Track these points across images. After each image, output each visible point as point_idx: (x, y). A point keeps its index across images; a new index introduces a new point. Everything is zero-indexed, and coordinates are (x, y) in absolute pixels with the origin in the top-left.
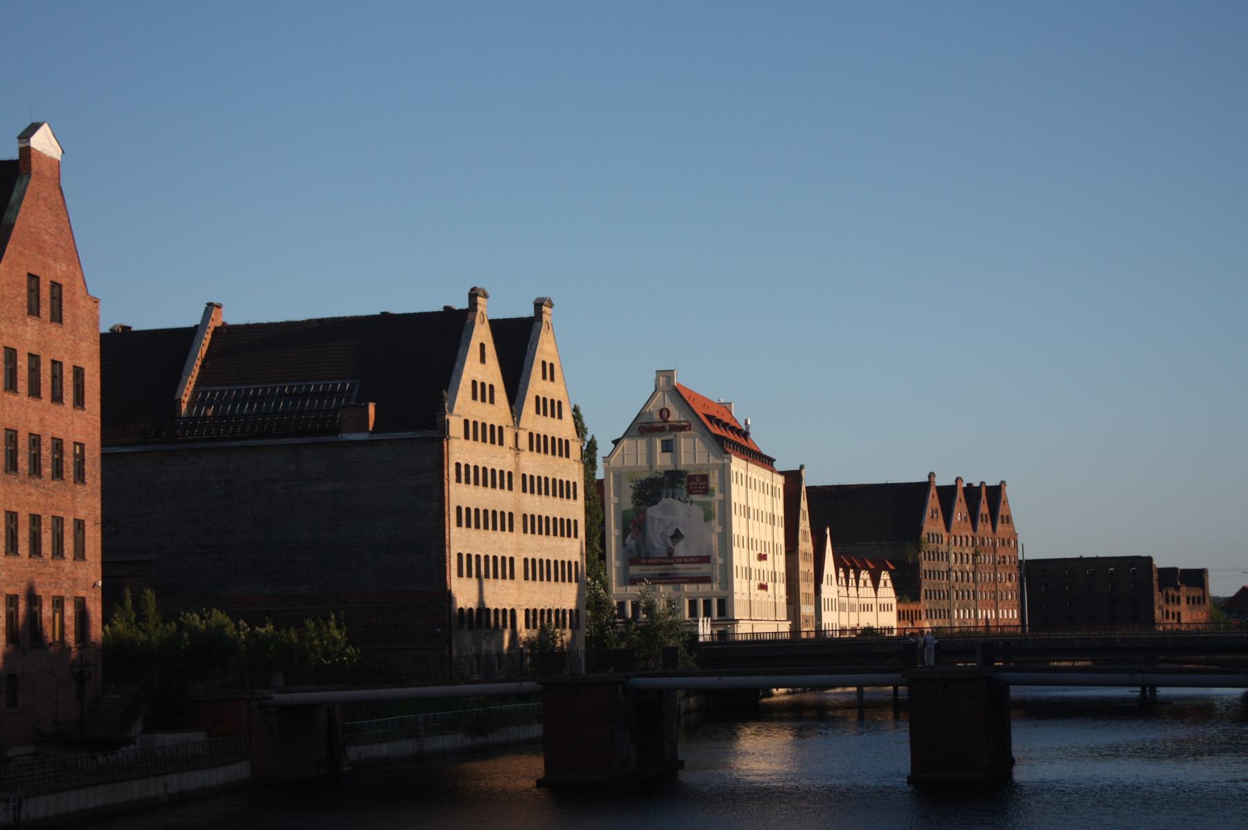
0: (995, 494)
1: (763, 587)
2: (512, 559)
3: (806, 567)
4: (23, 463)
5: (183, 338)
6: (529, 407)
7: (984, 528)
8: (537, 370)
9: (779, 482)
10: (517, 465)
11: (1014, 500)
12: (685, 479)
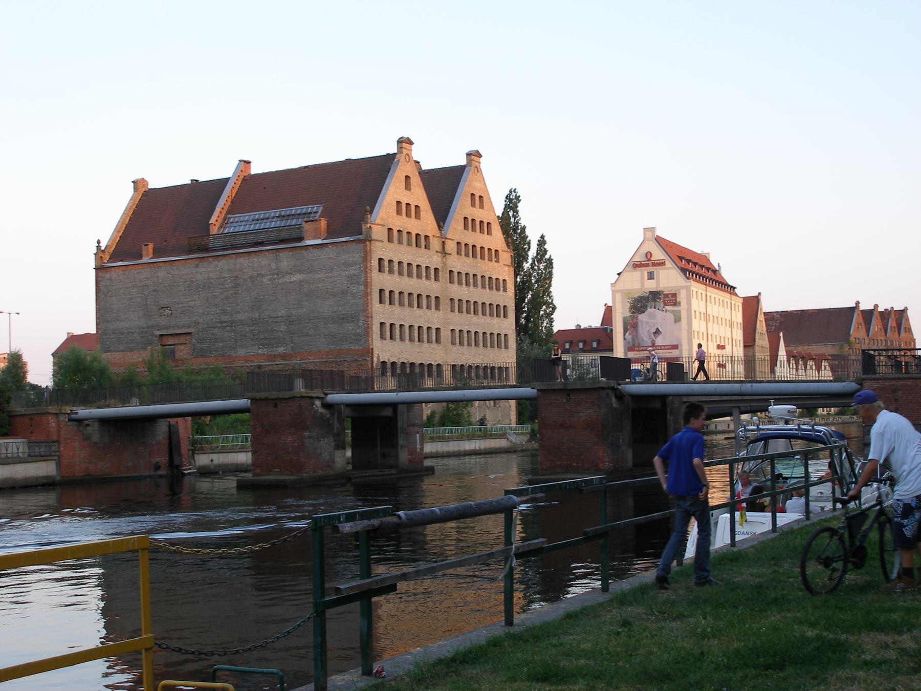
0: (902, 314)
5: (220, 185)
9: (739, 304)
10: (445, 264)
12: (662, 296)
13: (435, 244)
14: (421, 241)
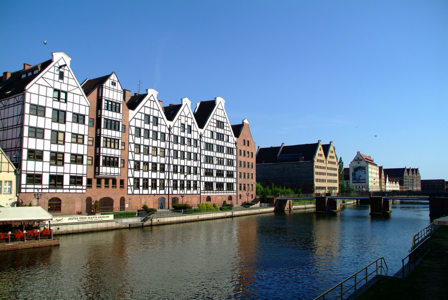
0: (417, 170)
1: (374, 184)
2: (325, 180)
3: (383, 181)
4: (242, 165)
5: (278, 148)
6: (328, 157)
7: (415, 175)
8: (330, 152)
9: (378, 168)
11: (420, 171)
13: (325, 162)
14: (322, 161)
